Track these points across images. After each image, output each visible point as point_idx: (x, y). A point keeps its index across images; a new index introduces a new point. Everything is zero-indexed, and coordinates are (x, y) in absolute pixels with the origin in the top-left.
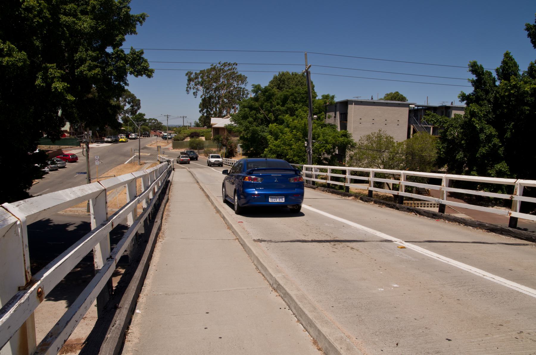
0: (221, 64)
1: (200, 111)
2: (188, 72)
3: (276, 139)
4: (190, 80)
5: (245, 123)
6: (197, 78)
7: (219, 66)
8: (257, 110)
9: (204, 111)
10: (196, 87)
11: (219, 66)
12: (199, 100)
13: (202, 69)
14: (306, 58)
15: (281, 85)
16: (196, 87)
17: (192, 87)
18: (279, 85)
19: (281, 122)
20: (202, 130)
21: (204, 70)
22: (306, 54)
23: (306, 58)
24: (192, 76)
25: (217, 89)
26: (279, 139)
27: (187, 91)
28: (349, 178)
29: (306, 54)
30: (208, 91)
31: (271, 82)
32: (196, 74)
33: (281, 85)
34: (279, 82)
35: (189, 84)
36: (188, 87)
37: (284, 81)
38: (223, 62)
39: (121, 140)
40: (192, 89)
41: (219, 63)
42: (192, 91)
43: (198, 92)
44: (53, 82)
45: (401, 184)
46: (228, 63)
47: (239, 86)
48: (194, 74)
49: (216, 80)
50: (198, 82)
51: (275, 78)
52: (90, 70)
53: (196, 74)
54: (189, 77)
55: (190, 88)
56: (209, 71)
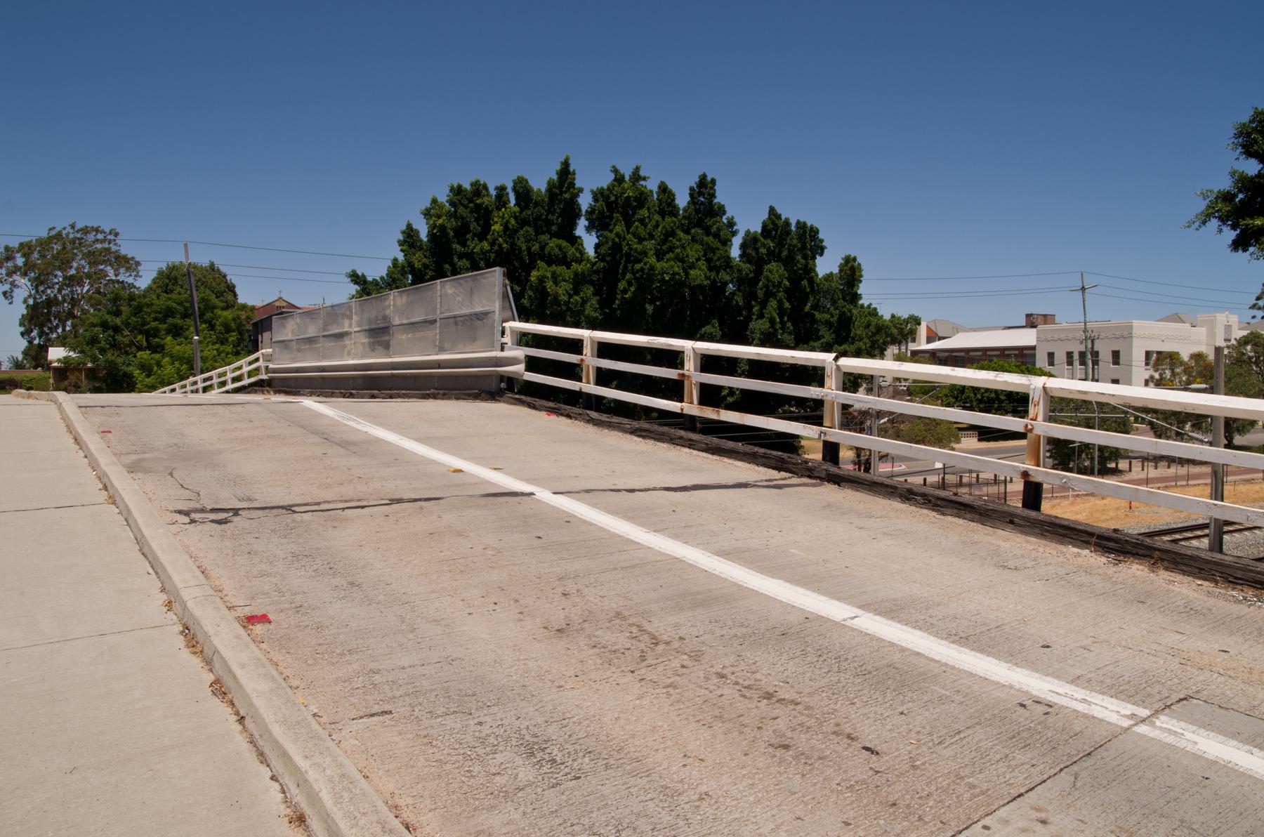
0: (76, 229)
1: (22, 334)
3: (148, 376)
9: (32, 334)
10: (11, 279)
12: (20, 310)
14: (186, 251)
15: (170, 286)
16: (11, 279)
18: (167, 285)
19: (155, 349)
20: (28, 374)
22: (186, 245)
23: (186, 251)
28: (593, 367)
29: (186, 245)
30: (41, 288)
31: (154, 281)
33: (170, 286)
34: (168, 281)
37: (176, 279)
43: (15, 290)
45: (586, 362)
47: (121, 278)
49: (65, 264)
50: (16, 266)
51: (161, 273)
56: (45, 244)
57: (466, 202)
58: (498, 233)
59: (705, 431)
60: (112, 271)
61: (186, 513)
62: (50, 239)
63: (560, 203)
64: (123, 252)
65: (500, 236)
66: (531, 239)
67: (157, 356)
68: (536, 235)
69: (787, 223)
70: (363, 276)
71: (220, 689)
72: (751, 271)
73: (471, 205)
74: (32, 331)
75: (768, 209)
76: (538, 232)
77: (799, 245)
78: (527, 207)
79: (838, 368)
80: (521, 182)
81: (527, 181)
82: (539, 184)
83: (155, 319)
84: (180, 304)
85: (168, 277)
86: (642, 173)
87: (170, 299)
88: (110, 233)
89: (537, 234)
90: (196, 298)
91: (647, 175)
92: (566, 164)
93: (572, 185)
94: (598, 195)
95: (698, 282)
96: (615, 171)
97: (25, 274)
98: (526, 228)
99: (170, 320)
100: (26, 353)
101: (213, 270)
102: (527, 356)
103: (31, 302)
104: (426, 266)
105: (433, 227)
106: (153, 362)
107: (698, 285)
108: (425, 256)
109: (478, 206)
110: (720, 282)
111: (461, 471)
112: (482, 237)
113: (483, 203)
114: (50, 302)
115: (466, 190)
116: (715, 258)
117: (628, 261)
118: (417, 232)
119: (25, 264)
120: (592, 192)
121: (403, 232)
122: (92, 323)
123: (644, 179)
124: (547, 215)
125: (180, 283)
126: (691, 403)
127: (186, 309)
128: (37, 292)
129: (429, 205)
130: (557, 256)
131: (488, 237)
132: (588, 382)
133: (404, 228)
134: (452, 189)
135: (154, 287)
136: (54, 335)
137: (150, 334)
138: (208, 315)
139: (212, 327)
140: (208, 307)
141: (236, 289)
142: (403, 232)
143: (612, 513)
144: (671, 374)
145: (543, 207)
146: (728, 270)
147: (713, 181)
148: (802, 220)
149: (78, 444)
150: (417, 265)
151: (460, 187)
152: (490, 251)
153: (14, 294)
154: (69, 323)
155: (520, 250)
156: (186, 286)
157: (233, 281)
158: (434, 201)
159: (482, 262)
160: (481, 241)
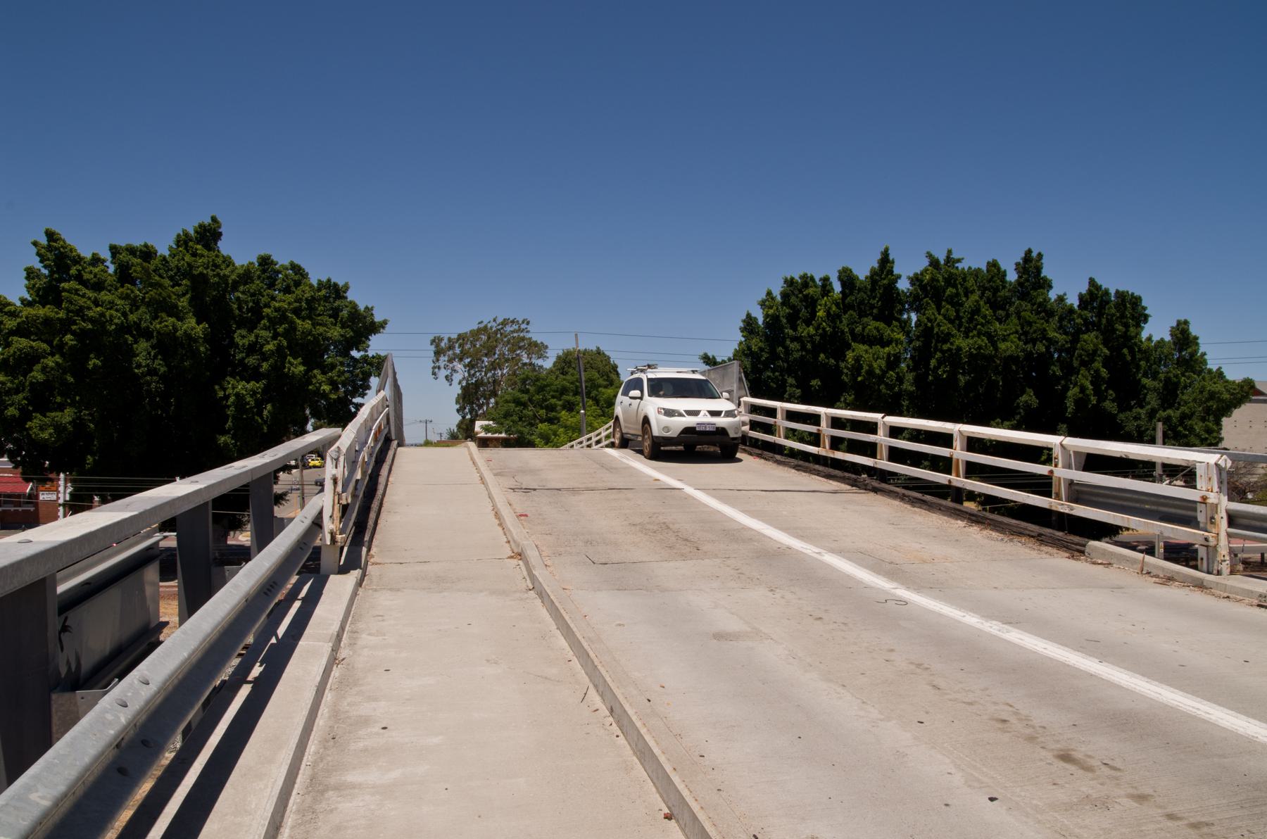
1: (458, 411)
2: (435, 337)
4: (438, 353)
5: (508, 422)
6: (451, 347)
7: (494, 324)
8: (524, 405)
10: (451, 365)
11: (494, 324)
12: (456, 390)
13: (462, 331)
17: (442, 366)
21: (466, 333)
22: (576, 335)
24: (443, 344)
25: (494, 366)
26: (551, 442)
27: (434, 374)
29: (576, 335)
30: (472, 372)
32: (450, 339)
35: (438, 360)
36: (434, 368)
37: (570, 362)
38: (500, 320)
39: (312, 463)
40: (443, 370)
41: (494, 320)
42: (443, 373)
43: (454, 374)
44: (321, 386)
46: (511, 319)
48: (446, 341)
49: (490, 351)
50: (454, 354)
52: (339, 376)
53: (450, 339)
54: (437, 346)
55: (439, 368)
56: (476, 334)
57: (796, 292)
58: (822, 318)
59: (825, 465)
60: (526, 355)
61: (513, 489)
62: (479, 330)
63: (880, 289)
64: (534, 339)
65: (824, 321)
66: (855, 322)
67: (554, 427)
68: (860, 318)
69: (1107, 293)
70: (714, 357)
71: (500, 525)
72: (1067, 342)
73: (800, 295)
74: (465, 408)
75: (1088, 281)
76: (862, 314)
77: (1118, 314)
78: (851, 294)
79: (884, 423)
80: (846, 272)
81: (851, 271)
82: (862, 272)
83: (553, 397)
84: (572, 383)
85: (565, 361)
86: (955, 256)
87: (564, 380)
88: (523, 322)
89: (860, 316)
90: (583, 379)
91: (961, 257)
92: (885, 255)
93: (891, 272)
94: (915, 280)
95: (1009, 353)
96: (929, 255)
97: (461, 360)
98: (851, 312)
99: (565, 397)
100: (459, 426)
101: (599, 353)
102: (751, 421)
103: (464, 383)
104: (761, 349)
105: (766, 316)
106: (550, 432)
107: (1009, 356)
108: (761, 341)
109: (806, 296)
110: (1037, 353)
111: (659, 480)
112: (808, 323)
113: (809, 293)
114: (479, 384)
115: (797, 282)
116: (1031, 331)
117: (938, 341)
118: (756, 319)
119: (462, 352)
120: (909, 278)
121: (744, 321)
122: (506, 400)
123: (959, 261)
124: (869, 300)
125: (573, 366)
126: (824, 447)
127: (577, 387)
128: (469, 375)
129: (765, 297)
130: (875, 337)
131: (813, 322)
132: (780, 437)
133: (744, 317)
134: (786, 281)
135: (554, 369)
136: (481, 411)
137: (552, 408)
138: (594, 393)
139: (597, 402)
140: (593, 385)
141: (618, 369)
142: (744, 321)
143: (743, 511)
144: (813, 429)
145: (865, 293)
146: (1044, 341)
147: (1040, 256)
148: (1121, 289)
149: (499, 519)
150: (754, 348)
151: (792, 279)
152: (814, 335)
153: (453, 378)
154: (492, 400)
155: (843, 332)
156: (577, 369)
157: (616, 362)
158: (769, 293)
159: (809, 344)
160: (808, 326)
